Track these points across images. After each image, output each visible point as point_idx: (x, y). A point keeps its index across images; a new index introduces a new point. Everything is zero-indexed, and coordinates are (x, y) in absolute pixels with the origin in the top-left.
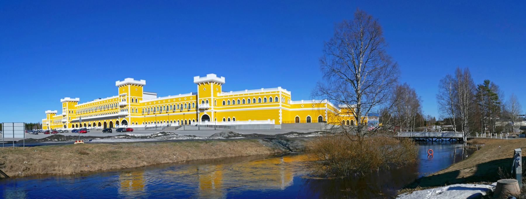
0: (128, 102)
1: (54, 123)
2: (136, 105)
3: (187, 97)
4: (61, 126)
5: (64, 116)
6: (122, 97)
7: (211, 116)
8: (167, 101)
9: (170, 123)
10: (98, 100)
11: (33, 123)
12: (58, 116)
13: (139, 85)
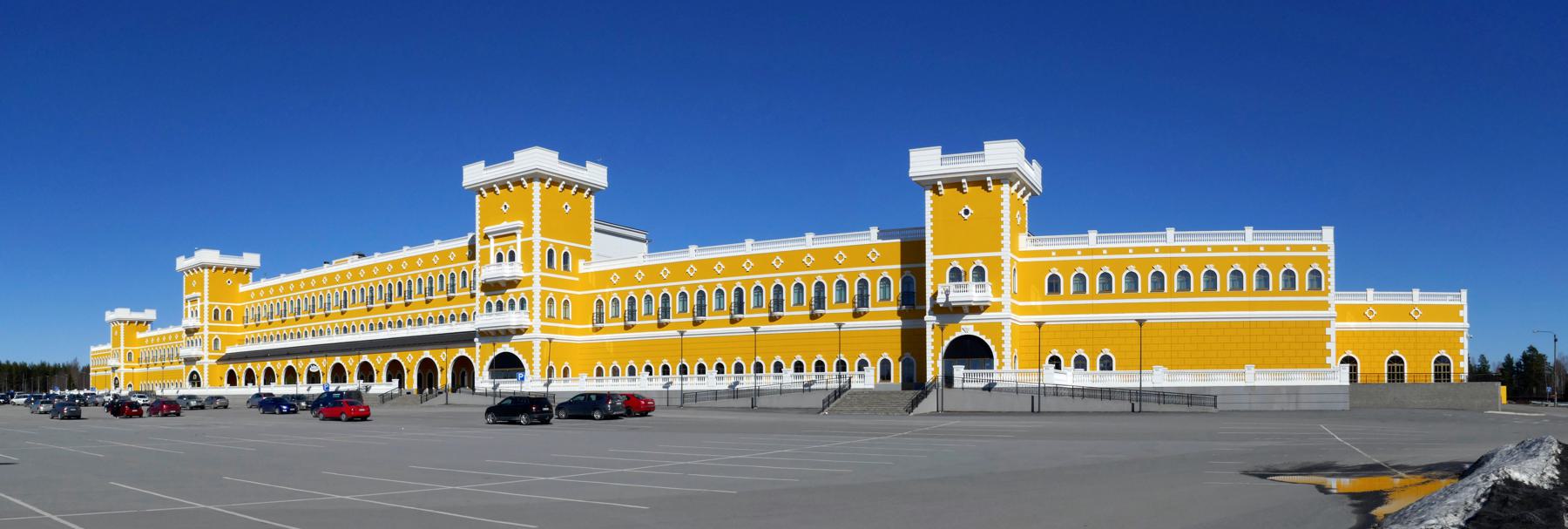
0: (528, 266)
1: (145, 361)
2: (229, 329)
3: (868, 251)
4: (178, 374)
5: (190, 332)
6: (492, 244)
7: (999, 343)
8: (734, 265)
9: (852, 371)
10: (353, 262)
11: (51, 361)
12: (160, 332)
13: (581, 189)
